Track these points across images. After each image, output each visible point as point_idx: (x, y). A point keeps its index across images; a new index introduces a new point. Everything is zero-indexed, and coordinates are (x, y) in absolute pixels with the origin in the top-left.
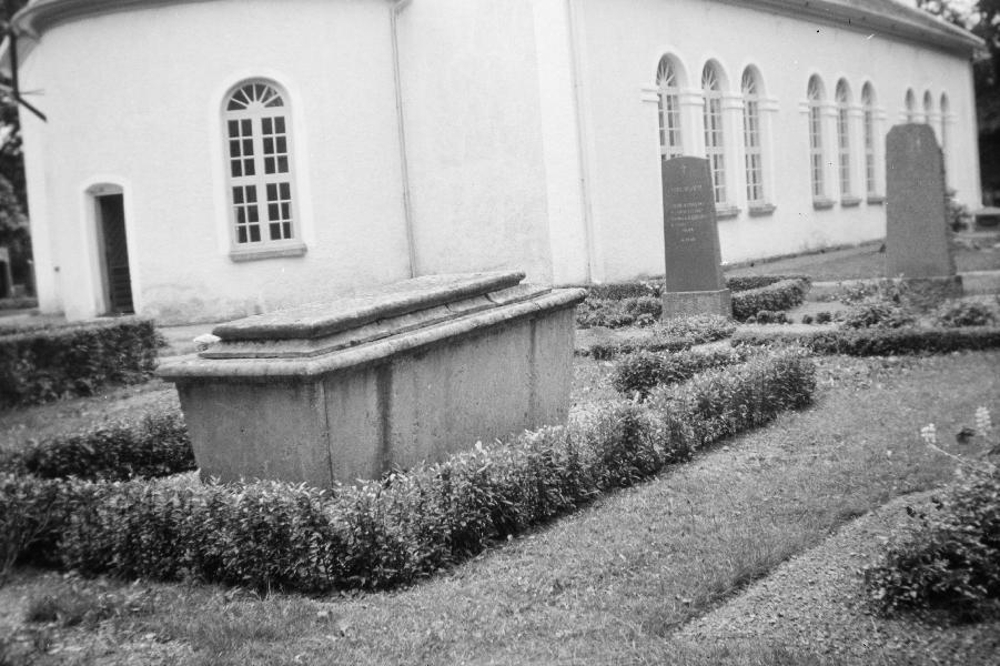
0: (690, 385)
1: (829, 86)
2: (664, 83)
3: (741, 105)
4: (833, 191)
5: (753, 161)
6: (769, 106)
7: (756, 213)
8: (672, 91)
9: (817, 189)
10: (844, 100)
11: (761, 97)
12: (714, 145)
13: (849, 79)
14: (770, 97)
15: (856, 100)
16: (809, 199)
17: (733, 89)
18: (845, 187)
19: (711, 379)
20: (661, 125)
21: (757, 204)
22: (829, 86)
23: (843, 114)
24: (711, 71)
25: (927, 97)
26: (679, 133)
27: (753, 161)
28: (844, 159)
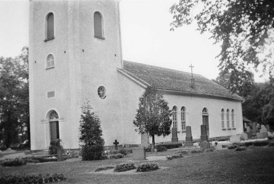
0: (111, 166)
1: (230, 110)
2: (182, 110)
3: (231, 114)
4: (226, 127)
5: (233, 122)
6: (187, 113)
7: (233, 129)
8: (184, 112)
9: (223, 126)
10: (223, 112)
11: (186, 112)
12: (203, 116)
13: (229, 109)
14: (235, 113)
15: (230, 112)
16: (222, 128)
17: (230, 112)
18: (228, 126)
19: (43, 177)
20: (182, 117)
21: (223, 128)
22: (230, 110)
23: (228, 115)
24: (228, 110)
25: (228, 110)
26: (177, 118)
27: (233, 122)
28: (228, 122)
